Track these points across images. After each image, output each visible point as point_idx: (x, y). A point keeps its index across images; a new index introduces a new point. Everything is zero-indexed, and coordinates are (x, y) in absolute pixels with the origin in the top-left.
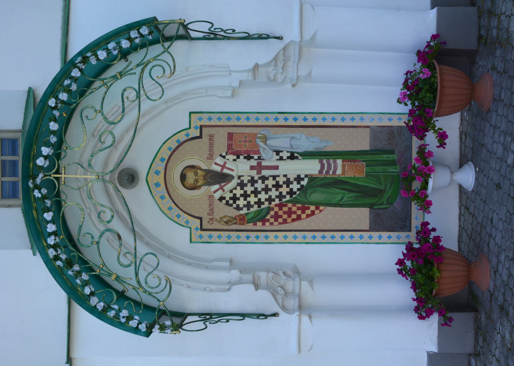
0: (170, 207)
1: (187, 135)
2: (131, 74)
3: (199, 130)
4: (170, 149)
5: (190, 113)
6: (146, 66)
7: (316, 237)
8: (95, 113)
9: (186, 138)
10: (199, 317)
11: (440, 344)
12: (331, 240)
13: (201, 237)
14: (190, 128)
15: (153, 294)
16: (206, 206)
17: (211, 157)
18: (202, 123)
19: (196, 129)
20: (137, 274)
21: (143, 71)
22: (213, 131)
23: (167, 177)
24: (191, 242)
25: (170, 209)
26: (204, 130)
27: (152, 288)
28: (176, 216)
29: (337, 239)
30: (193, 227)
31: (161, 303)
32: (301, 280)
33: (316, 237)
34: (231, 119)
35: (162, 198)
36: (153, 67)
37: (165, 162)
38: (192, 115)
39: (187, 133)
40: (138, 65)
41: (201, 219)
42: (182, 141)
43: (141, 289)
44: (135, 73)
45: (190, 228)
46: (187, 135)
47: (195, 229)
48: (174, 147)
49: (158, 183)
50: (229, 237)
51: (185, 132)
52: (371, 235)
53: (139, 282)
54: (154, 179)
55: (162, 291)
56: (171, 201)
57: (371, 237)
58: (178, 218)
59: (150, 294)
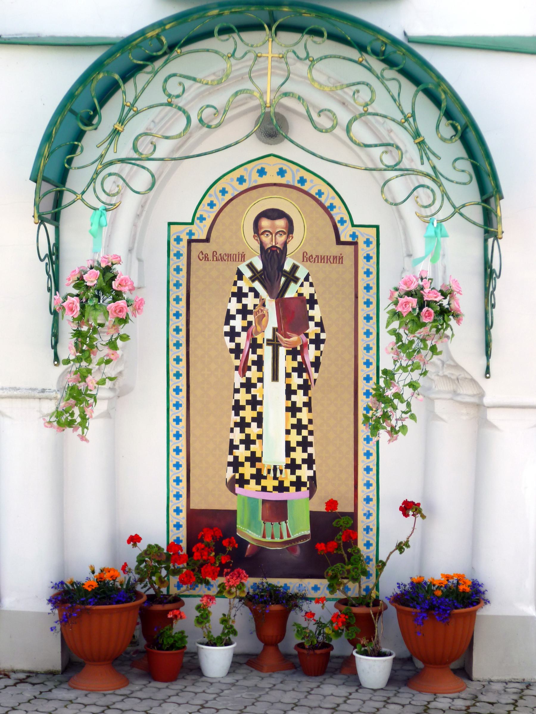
0: (227, 192)
1: (342, 221)
2: (422, 158)
3: (350, 239)
4: (320, 193)
5: (377, 227)
6: (434, 180)
7: (178, 454)
8: (363, 104)
9: (337, 218)
10: (54, 245)
11: (9, 612)
12: (172, 447)
13: (178, 240)
14: (353, 225)
15: (92, 184)
16: (227, 249)
17: (307, 258)
18: (361, 245)
19: (351, 236)
20: (122, 161)
21: (427, 175)
22: (349, 262)
23: (274, 188)
24: (170, 224)
25: (224, 192)
26: (350, 249)
27: (102, 184)
28: (212, 202)
29: (174, 458)
30: (194, 228)
31: (79, 196)
32: (109, 399)
33: (178, 454)
34: (368, 291)
35: (241, 180)
36: (432, 191)
37: (299, 185)
38: (375, 229)
39: (345, 222)
40: (434, 168)
41: (207, 240)
42: (332, 212)
43: (100, 166)
44: (422, 164)
45: (192, 223)
46: (342, 221)
47: (190, 231)
48: (322, 199)
49: (265, 173)
50: (178, 285)
51: (346, 218)
52: (181, 511)
53: (111, 163)
54: (272, 167)
55: (97, 197)
56: (236, 193)
57: (178, 511)
58: (208, 205)
59: (93, 180)
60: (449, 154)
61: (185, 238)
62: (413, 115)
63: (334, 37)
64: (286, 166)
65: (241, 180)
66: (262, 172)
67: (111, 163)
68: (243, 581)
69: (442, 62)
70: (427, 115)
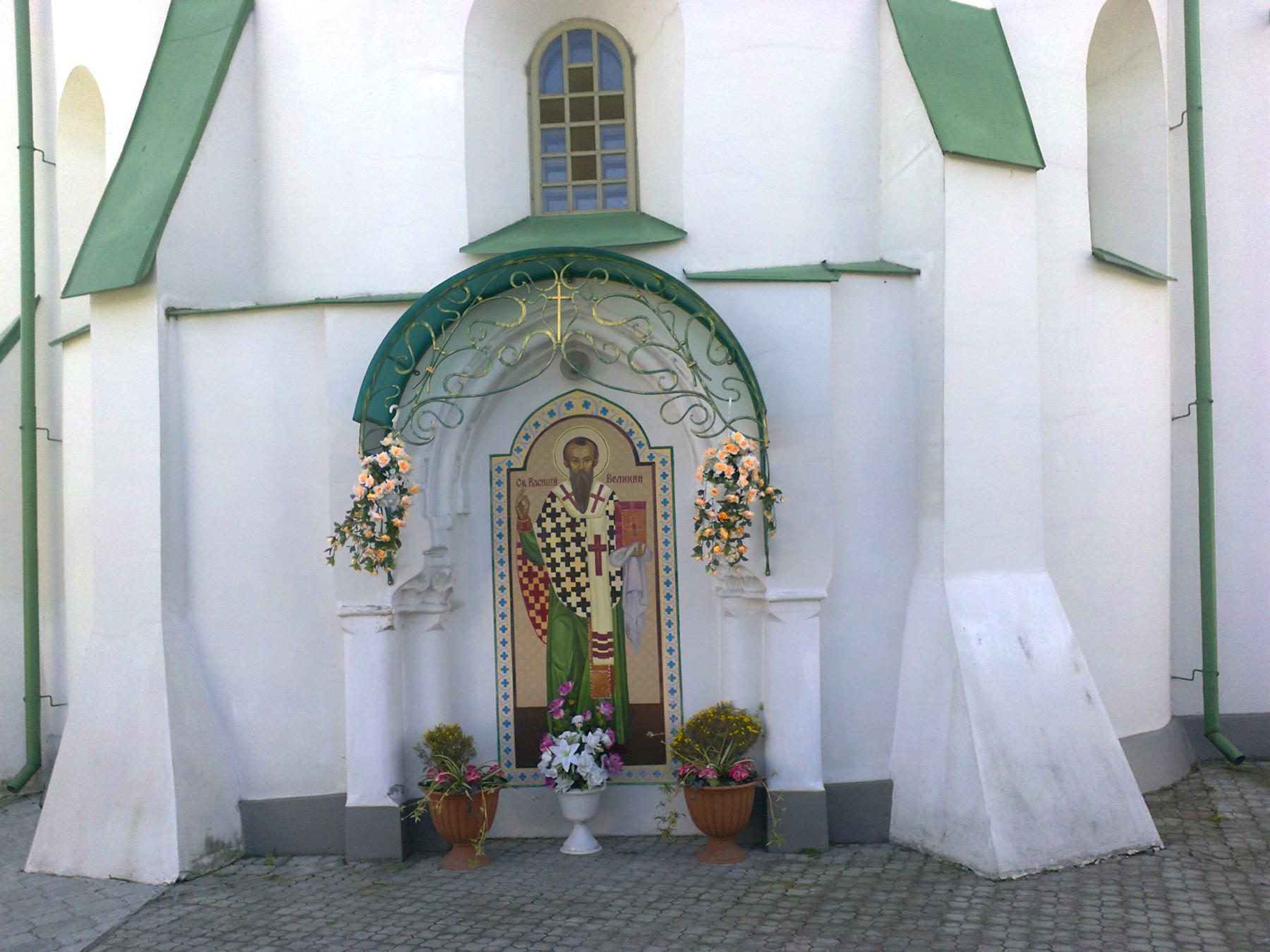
1: (640, 445)
4: (620, 421)
5: (671, 448)
9: (636, 443)
13: (499, 470)
16: (541, 475)
18: (658, 465)
21: (700, 395)
22: (647, 480)
23: (582, 419)
24: (492, 456)
30: (512, 459)
35: (551, 414)
41: (524, 469)
51: (644, 442)
53: (424, 402)
54: (578, 399)
60: (720, 374)
61: (505, 467)
62: (686, 343)
63: (615, 278)
64: (590, 399)
65: (551, 414)
66: (569, 405)
67: (424, 402)
68: (471, 763)
69: (712, 296)
70: (699, 339)
